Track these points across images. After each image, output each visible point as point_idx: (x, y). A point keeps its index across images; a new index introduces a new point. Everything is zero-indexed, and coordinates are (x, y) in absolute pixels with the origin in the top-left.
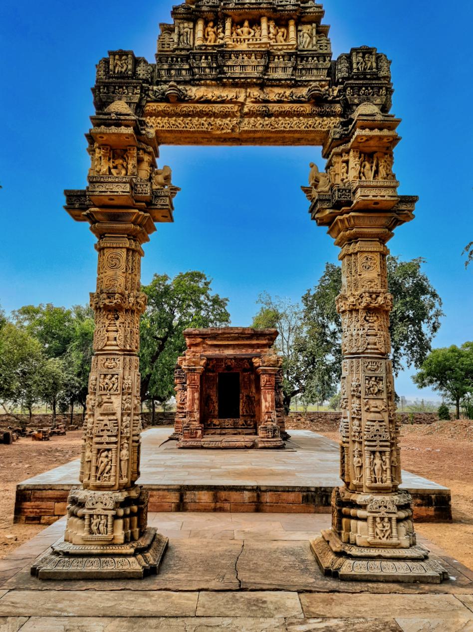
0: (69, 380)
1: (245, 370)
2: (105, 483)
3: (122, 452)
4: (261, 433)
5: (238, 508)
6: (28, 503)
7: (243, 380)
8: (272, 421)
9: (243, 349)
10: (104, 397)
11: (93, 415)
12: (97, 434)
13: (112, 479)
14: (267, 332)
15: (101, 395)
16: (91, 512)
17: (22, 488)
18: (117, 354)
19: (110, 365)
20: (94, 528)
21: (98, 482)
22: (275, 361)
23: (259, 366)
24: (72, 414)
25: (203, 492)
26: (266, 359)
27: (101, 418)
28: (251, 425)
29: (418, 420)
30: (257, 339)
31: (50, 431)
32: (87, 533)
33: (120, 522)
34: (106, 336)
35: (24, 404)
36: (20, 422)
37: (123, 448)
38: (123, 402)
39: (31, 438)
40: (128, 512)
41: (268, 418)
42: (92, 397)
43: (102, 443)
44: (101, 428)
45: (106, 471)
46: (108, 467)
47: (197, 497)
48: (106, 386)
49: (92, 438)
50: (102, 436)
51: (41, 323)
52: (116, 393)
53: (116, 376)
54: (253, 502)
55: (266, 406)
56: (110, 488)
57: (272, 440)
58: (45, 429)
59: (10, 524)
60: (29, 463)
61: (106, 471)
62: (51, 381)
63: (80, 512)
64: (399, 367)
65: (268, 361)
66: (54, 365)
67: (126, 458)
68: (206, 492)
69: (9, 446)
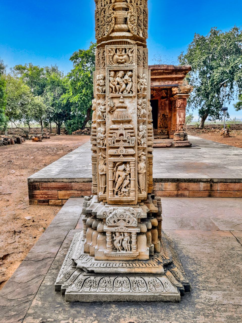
0: (48, 109)
1: (163, 98)
2: (125, 199)
3: (139, 165)
4: (176, 138)
5: (195, 195)
6: (38, 191)
7: (161, 105)
8: (183, 130)
9: (165, 81)
10: (116, 101)
11: (105, 124)
12: (112, 145)
13: (132, 194)
14: (184, 68)
15: (112, 98)
16: (113, 229)
17: (32, 181)
18: (129, 43)
19: (121, 58)
20: (118, 246)
21: (117, 198)
22: (188, 89)
23: (177, 93)
24: (51, 128)
25: (168, 183)
26: (181, 88)
27: (115, 126)
28: (166, 133)
29: (231, 128)
30: (176, 74)
31: (41, 137)
32: (111, 250)
33: (143, 238)
34: (113, 16)
35: (25, 122)
36: (25, 132)
37: (140, 160)
38: (139, 107)
39: (32, 141)
40: (150, 227)
41: (181, 128)
42: (101, 101)
43: (119, 156)
44: (116, 139)
45: (124, 185)
46: (127, 182)
47: (164, 186)
48: (117, 87)
49: (105, 150)
50: (118, 148)
51: (27, 75)
52: (131, 95)
53: (130, 73)
54: (206, 190)
55: (180, 121)
56: (129, 203)
57: (183, 142)
58: (39, 135)
59: (27, 205)
60: (33, 156)
61: (124, 185)
62: (38, 108)
63: (100, 226)
64: (232, 98)
65: (184, 90)
66: (39, 100)
67: (145, 171)
68: (170, 183)
69: (20, 145)
